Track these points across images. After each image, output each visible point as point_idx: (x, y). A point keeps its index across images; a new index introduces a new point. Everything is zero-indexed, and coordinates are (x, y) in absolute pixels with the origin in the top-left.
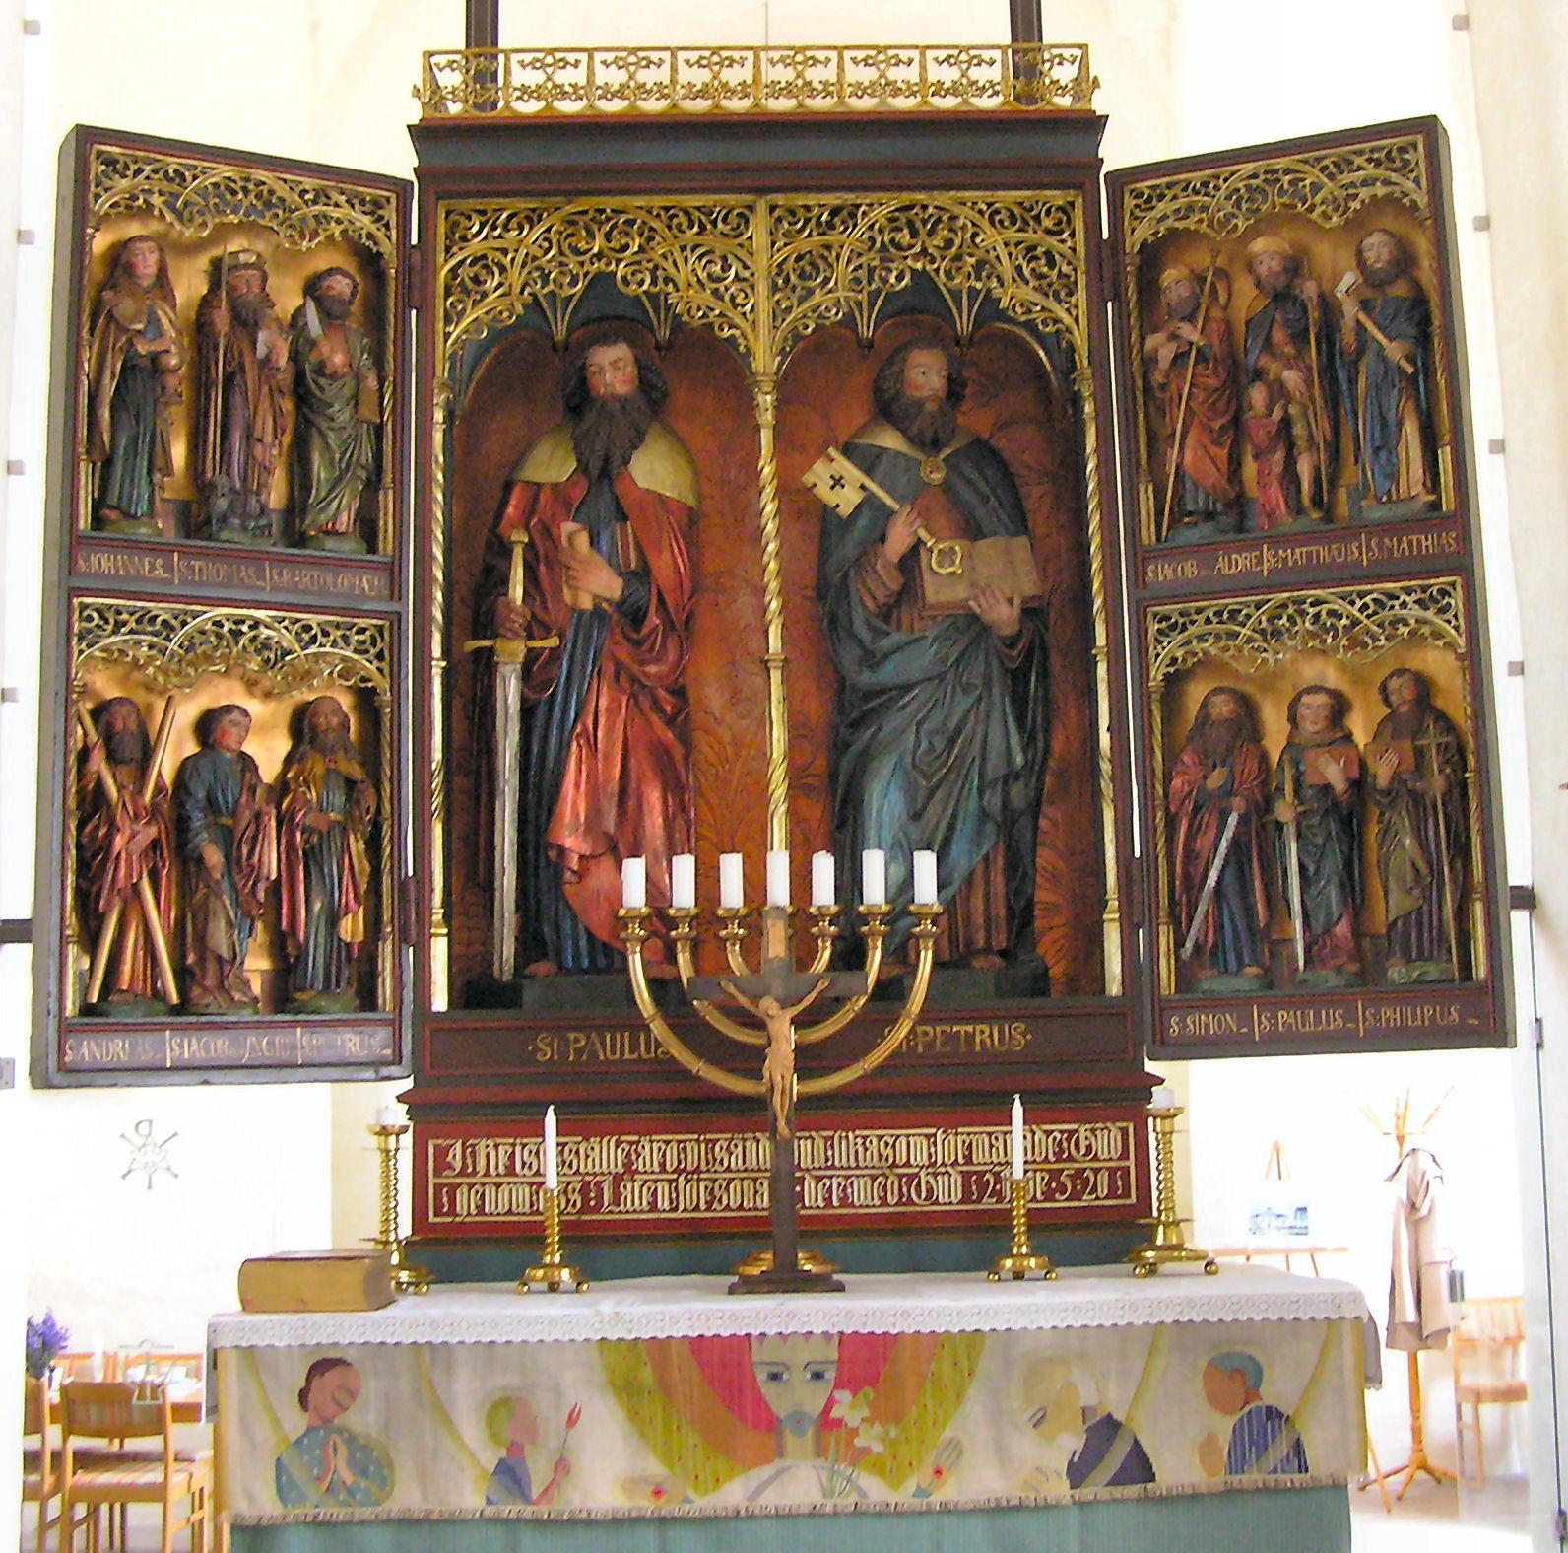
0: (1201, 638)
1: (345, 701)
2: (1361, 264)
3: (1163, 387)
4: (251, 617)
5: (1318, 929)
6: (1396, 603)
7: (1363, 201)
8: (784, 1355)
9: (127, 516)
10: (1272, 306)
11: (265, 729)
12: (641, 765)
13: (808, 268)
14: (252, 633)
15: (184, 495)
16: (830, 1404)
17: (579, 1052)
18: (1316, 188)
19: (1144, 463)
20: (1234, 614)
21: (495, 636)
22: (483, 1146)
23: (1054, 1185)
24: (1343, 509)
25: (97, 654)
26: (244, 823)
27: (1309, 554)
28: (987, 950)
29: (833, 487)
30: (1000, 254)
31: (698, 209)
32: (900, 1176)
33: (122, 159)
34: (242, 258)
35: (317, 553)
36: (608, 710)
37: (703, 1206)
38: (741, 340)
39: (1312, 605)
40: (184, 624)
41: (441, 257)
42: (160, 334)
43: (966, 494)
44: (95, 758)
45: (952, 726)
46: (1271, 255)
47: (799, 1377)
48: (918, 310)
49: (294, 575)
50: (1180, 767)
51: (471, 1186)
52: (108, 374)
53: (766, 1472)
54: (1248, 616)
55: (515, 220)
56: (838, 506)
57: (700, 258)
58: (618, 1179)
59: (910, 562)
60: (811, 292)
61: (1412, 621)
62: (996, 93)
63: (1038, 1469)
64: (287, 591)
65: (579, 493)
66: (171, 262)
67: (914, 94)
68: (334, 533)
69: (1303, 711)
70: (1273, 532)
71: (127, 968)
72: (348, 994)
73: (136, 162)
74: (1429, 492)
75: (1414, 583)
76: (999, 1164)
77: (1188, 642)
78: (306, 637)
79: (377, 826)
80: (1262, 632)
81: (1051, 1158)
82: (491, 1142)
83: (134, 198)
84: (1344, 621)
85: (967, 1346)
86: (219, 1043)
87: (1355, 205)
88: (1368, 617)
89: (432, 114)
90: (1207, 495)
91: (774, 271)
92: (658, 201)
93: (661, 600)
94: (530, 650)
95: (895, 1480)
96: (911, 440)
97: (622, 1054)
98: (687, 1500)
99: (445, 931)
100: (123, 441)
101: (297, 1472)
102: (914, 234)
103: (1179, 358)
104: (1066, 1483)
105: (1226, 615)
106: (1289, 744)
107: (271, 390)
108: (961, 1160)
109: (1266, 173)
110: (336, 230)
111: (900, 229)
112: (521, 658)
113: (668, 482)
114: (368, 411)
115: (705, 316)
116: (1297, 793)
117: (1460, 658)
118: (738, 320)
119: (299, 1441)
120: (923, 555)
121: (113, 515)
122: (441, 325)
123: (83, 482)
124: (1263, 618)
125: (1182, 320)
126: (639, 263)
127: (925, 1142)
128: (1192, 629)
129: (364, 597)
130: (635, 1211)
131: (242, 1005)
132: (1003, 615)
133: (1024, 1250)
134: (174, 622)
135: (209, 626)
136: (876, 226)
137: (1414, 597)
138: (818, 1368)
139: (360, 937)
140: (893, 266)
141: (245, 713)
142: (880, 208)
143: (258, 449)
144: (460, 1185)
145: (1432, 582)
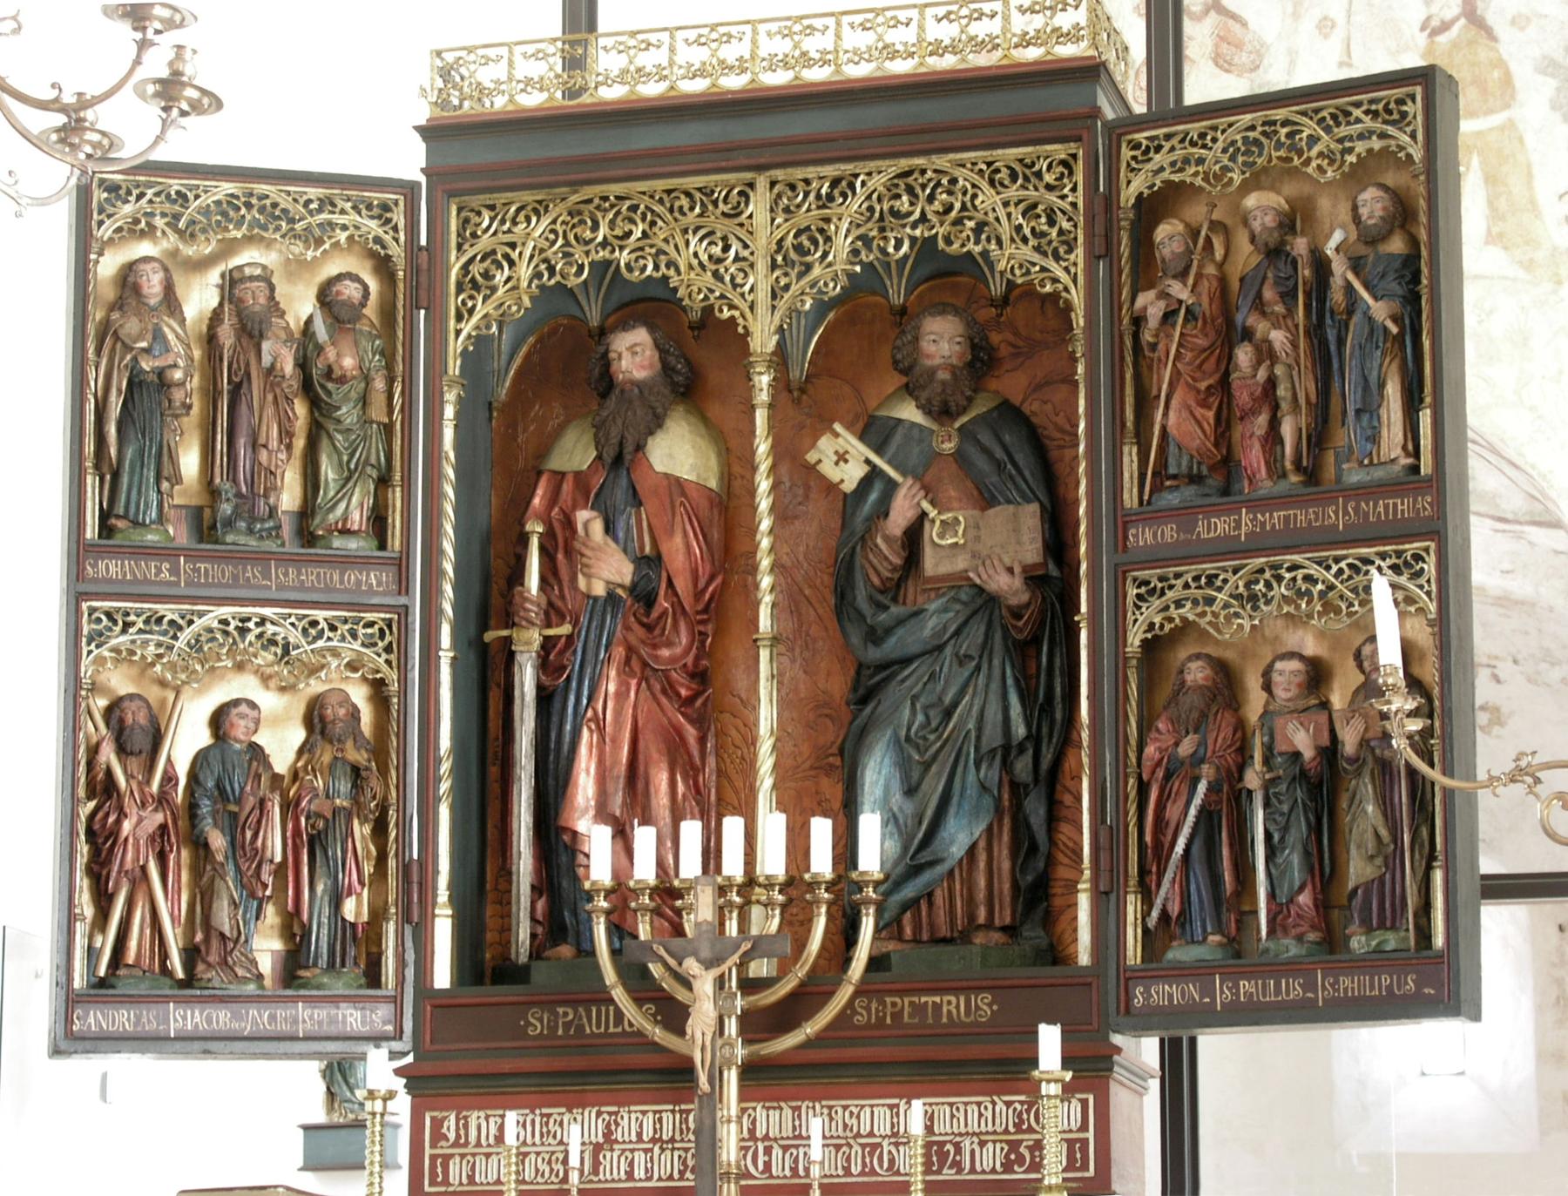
0: (1179, 604)
1: (359, 695)
2: (1356, 219)
3: (1153, 347)
4: (256, 615)
7: (1359, 155)
10: (1266, 263)
11: (276, 721)
12: (652, 748)
13: (806, 243)
14: (259, 630)
15: (194, 502)
17: (567, 1025)
18: (1313, 140)
19: (1129, 424)
20: (1211, 579)
22: (475, 1117)
23: (1013, 1157)
24: (1329, 472)
25: (107, 654)
26: (248, 809)
27: (1287, 518)
28: (989, 925)
29: (837, 463)
30: (1015, 223)
31: (700, 190)
32: (863, 1146)
34: (247, 271)
36: (618, 694)
37: (676, 1175)
38: (740, 321)
39: (1289, 570)
40: (191, 622)
41: (453, 258)
42: (168, 349)
43: (981, 463)
45: (948, 700)
46: (1264, 210)
48: (946, 275)
49: (299, 573)
50: (1153, 735)
51: (463, 1156)
52: (114, 391)
54: (1225, 581)
55: (523, 213)
56: (842, 481)
57: (701, 240)
59: (913, 536)
64: (294, 589)
65: (598, 481)
66: (178, 279)
67: (912, 55)
68: (345, 532)
69: (1276, 678)
70: (1254, 495)
71: (133, 944)
72: (353, 973)
73: (138, 186)
74: (1408, 455)
75: (1387, 548)
76: (961, 1135)
77: (1167, 608)
79: (383, 809)
80: (1238, 597)
81: (1011, 1129)
82: (482, 1114)
83: (137, 221)
84: (1320, 587)
86: (221, 1015)
87: (1351, 159)
89: (438, 112)
90: (1192, 457)
92: (660, 185)
93: (670, 583)
94: (546, 638)
96: (926, 409)
97: (607, 1027)
100: (129, 453)
103: (1168, 317)
105: (1203, 580)
106: (1265, 713)
107: (275, 397)
109: (1264, 124)
110: (343, 236)
111: (898, 196)
112: (536, 645)
113: (687, 467)
114: (377, 412)
115: (706, 298)
116: (1267, 761)
117: (1431, 624)
118: (737, 301)
120: (927, 525)
121: (121, 524)
122: (452, 322)
123: (89, 494)
124: (1241, 584)
125: (1174, 277)
126: (641, 249)
127: (888, 1112)
128: (1170, 594)
130: (613, 1180)
131: (245, 980)
132: (1006, 584)
134: (180, 621)
135: (215, 624)
136: (875, 196)
137: (1389, 562)
139: (365, 918)
140: (891, 235)
141: (253, 705)
142: (876, 177)
143: (263, 456)
144: (452, 1156)
145: (1407, 546)
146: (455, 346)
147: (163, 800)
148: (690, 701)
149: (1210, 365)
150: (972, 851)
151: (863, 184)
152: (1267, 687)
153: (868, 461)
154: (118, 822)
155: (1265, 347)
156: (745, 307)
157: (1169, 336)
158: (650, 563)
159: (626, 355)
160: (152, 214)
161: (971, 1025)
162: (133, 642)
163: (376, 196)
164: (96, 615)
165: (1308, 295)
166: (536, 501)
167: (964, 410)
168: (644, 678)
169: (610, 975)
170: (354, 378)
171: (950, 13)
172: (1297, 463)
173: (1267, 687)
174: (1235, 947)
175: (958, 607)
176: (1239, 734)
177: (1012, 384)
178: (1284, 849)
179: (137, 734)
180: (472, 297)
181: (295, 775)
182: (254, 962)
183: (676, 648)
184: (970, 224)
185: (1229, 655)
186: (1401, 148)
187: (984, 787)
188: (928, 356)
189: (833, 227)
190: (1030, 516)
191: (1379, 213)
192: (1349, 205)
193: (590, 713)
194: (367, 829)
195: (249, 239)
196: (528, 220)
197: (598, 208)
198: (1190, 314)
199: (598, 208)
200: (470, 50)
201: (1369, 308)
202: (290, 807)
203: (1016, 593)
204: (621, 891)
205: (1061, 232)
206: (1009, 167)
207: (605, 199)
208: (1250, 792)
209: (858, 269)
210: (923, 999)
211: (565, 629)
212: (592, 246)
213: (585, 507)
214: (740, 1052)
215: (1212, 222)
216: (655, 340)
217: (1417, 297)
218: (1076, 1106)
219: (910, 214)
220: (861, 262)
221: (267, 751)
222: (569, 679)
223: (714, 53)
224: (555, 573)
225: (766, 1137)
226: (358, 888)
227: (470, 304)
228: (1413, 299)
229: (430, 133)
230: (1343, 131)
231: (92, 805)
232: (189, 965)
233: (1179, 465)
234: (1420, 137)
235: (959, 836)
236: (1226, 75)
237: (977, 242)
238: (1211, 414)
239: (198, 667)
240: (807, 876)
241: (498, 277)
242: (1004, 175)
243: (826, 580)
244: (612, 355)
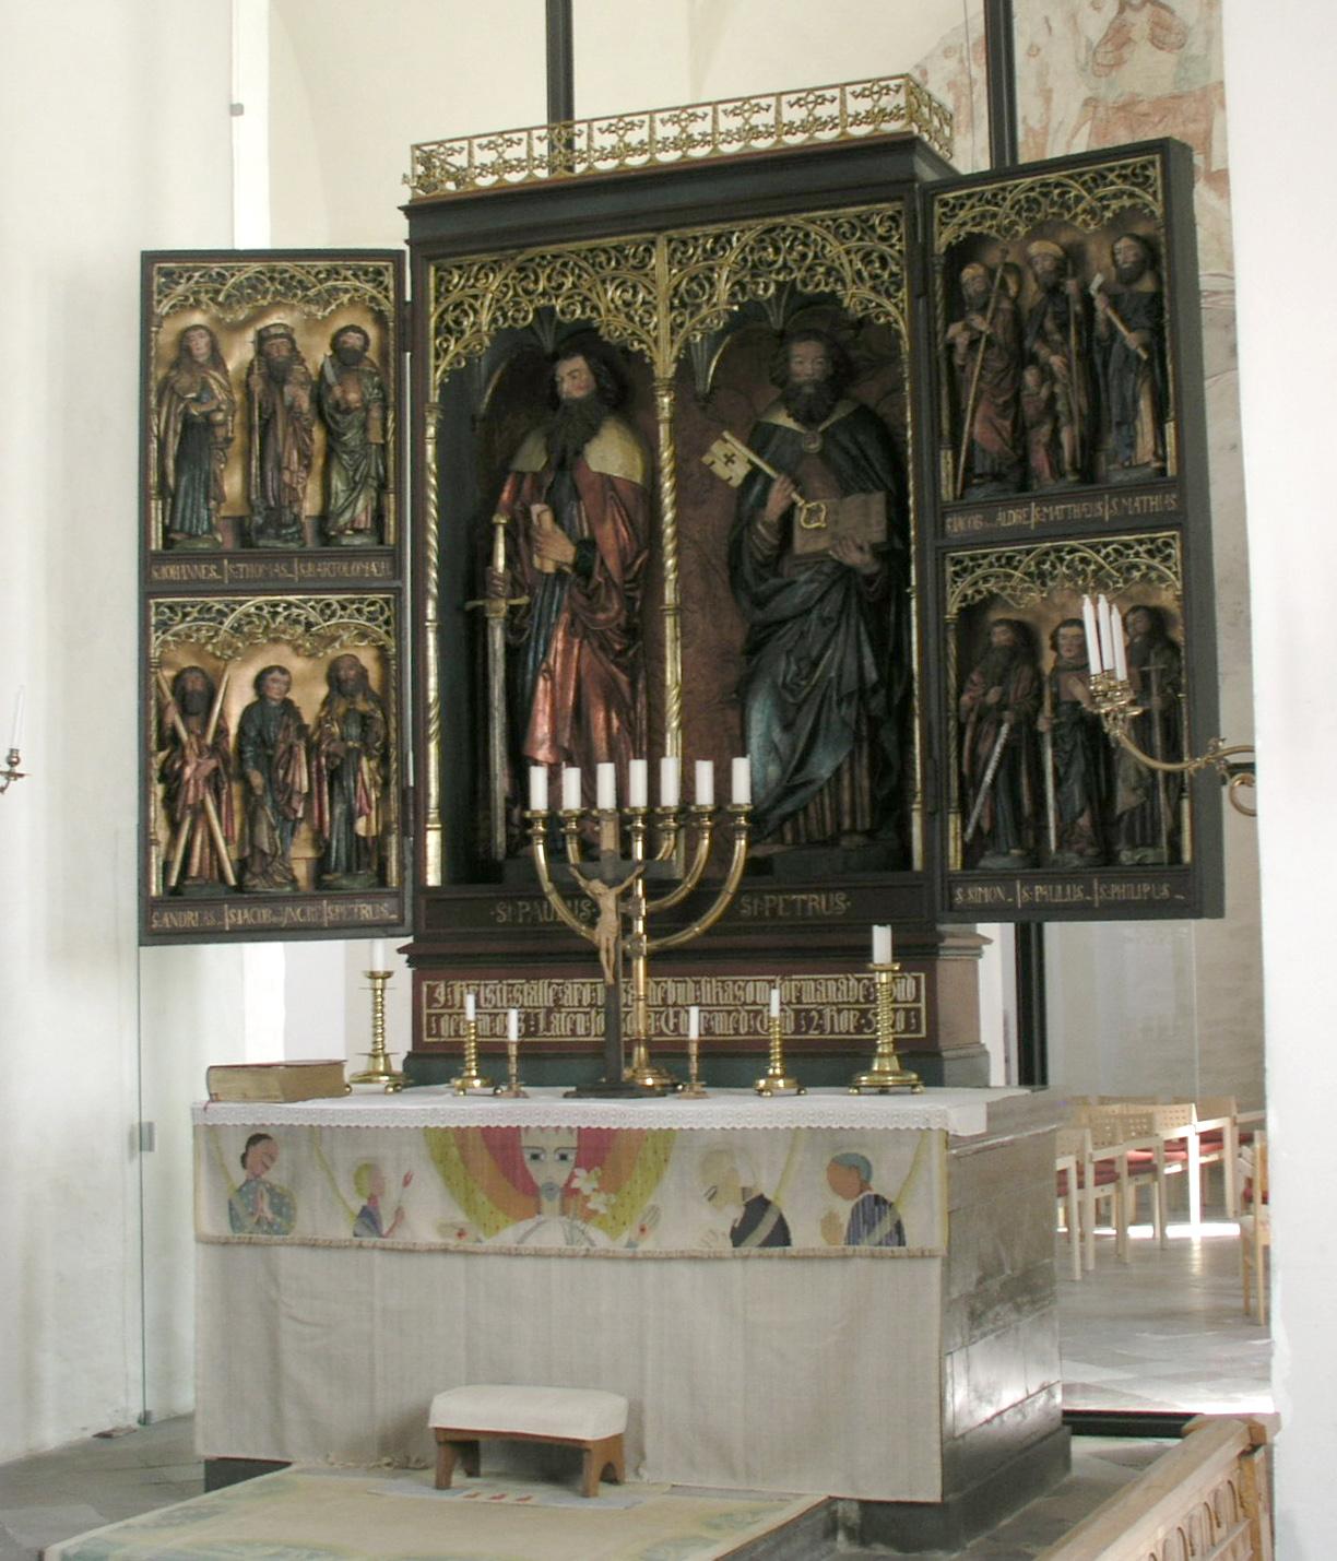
0: (986, 579)
1: (367, 658)
2: (1115, 262)
3: (963, 368)
4: (285, 602)
5: (1068, 819)
6: (1131, 552)
8: (541, 1141)
9: (191, 536)
11: (306, 680)
13: (696, 288)
15: (239, 513)
16: (572, 1177)
18: (1079, 199)
20: (1010, 559)
21: (484, 597)
23: (863, 1021)
25: (170, 638)
28: (853, 831)
30: (853, 264)
31: (614, 248)
32: (749, 1012)
33: (177, 271)
35: (334, 549)
36: (564, 650)
38: (648, 352)
39: (1069, 553)
40: (233, 610)
41: (432, 309)
42: (213, 397)
44: (174, 709)
45: (814, 653)
46: (1045, 256)
47: (550, 1157)
48: (812, 311)
49: (316, 567)
52: (171, 433)
53: (529, 1224)
54: (1020, 561)
55: (483, 272)
56: (731, 478)
58: (549, 1011)
59: (787, 519)
60: (699, 307)
61: (1143, 567)
62: (835, 126)
63: (712, 1232)
65: (548, 480)
67: (771, 135)
69: (1061, 641)
71: (196, 861)
75: (1143, 536)
76: (823, 1004)
77: (976, 583)
78: (328, 612)
79: (386, 746)
81: (862, 1000)
82: (464, 983)
83: (187, 298)
84: (1093, 567)
85: (664, 1141)
87: (1108, 214)
88: (1110, 563)
90: (993, 461)
91: (671, 292)
92: (585, 245)
94: (512, 607)
95: (614, 1233)
98: (479, 1241)
99: (438, 826)
101: (239, 1209)
102: (777, 251)
104: (729, 1243)
107: (295, 430)
108: (794, 1001)
109: (1042, 185)
110: (345, 298)
112: (503, 613)
113: (617, 467)
114: (375, 436)
115: (621, 335)
116: (1055, 707)
118: (645, 337)
119: (240, 1190)
120: (797, 512)
121: (177, 537)
124: (1032, 563)
128: (979, 572)
129: (373, 578)
133: (778, 1071)
134: (226, 610)
135: (253, 610)
136: (747, 249)
138: (564, 1152)
140: (761, 280)
141: (283, 671)
142: (743, 236)
143: (286, 477)
144: (442, 1015)
145: (1158, 535)
146: (436, 377)
147: (216, 749)
148: (621, 653)
149: (1006, 384)
150: (837, 772)
151: (738, 239)
152: (1055, 647)
153: (750, 462)
154: (182, 768)
155: (1047, 368)
156: (650, 341)
157: (974, 360)
158: (587, 547)
159: (567, 378)
160: (199, 292)
161: (829, 917)
162: (190, 628)
163: (371, 264)
164: (162, 608)
165: (1078, 324)
166: (505, 496)
167: (825, 417)
168: (585, 636)
169: (547, 886)
170: (357, 409)
171: (800, 99)
172: (1073, 463)
173: (1055, 647)
174: (1035, 859)
175: (822, 578)
176: (1036, 684)
177: (868, 391)
178: (1068, 779)
179: (195, 696)
180: (446, 340)
181: (320, 723)
182: (290, 870)
183: (611, 611)
184: (821, 270)
185: (1028, 618)
186: (1146, 206)
187: (844, 723)
188: (798, 375)
189: (716, 276)
190: (877, 502)
191: (1132, 259)
192: (1109, 250)
193: (544, 666)
194: (373, 764)
195: (276, 305)
196: (487, 276)
197: (539, 265)
198: (990, 343)
199: (539, 265)
200: (440, 144)
201: (1124, 338)
202: (313, 750)
203: (867, 565)
204: (554, 818)
205: (892, 275)
206: (849, 222)
207: (543, 257)
208: (1042, 734)
209: (736, 308)
210: (794, 897)
211: (523, 600)
212: (533, 297)
213: (539, 502)
214: (644, 945)
215: (1006, 264)
216: (590, 366)
217: (1161, 328)
218: (911, 983)
219: (775, 262)
220: (738, 303)
221: (297, 704)
222: (530, 636)
223: (621, 138)
224: (517, 553)
225: (675, 1005)
226: (367, 810)
227: (445, 345)
228: (1158, 331)
229: (411, 211)
230: (1101, 191)
231: (162, 755)
232: (239, 877)
233: (983, 466)
234: (1160, 197)
235: (824, 765)
236: (1159, 52)
237: (827, 284)
238: (1007, 424)
239: (240, 645)
240: (693, 808)
241: (465, 323)
242: (846, 228)
243: (723, 551)
244: (558, 379)
